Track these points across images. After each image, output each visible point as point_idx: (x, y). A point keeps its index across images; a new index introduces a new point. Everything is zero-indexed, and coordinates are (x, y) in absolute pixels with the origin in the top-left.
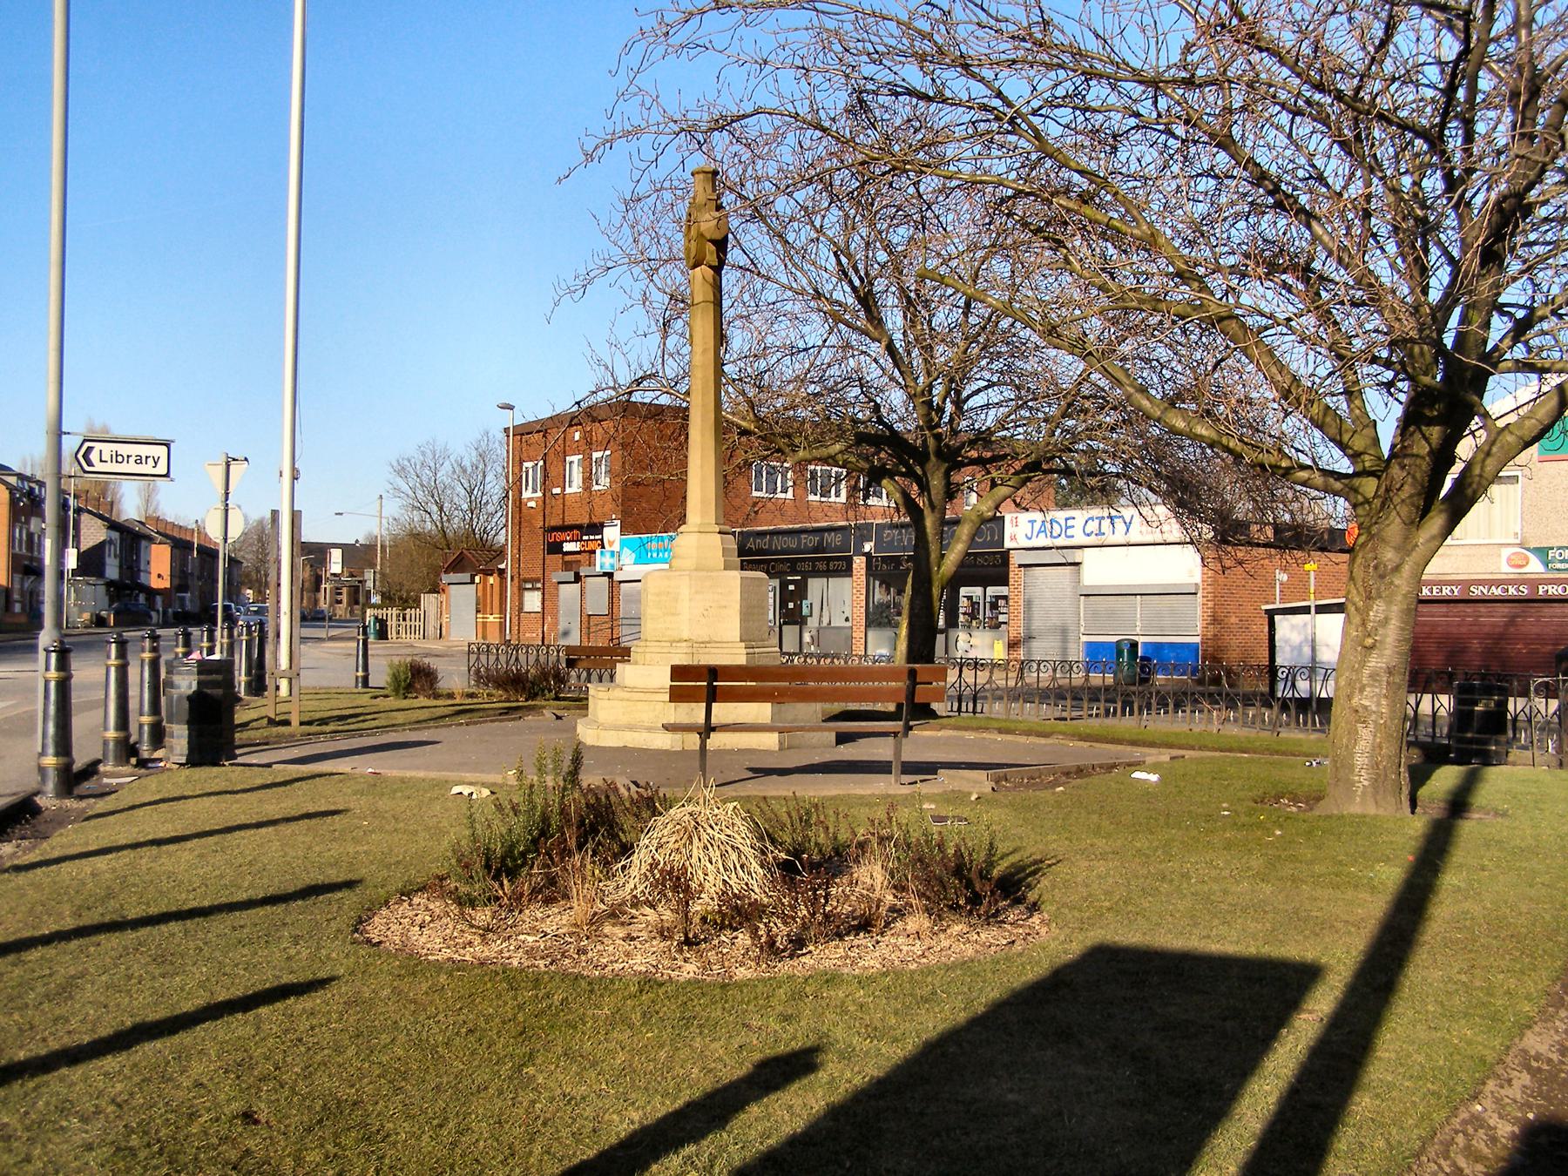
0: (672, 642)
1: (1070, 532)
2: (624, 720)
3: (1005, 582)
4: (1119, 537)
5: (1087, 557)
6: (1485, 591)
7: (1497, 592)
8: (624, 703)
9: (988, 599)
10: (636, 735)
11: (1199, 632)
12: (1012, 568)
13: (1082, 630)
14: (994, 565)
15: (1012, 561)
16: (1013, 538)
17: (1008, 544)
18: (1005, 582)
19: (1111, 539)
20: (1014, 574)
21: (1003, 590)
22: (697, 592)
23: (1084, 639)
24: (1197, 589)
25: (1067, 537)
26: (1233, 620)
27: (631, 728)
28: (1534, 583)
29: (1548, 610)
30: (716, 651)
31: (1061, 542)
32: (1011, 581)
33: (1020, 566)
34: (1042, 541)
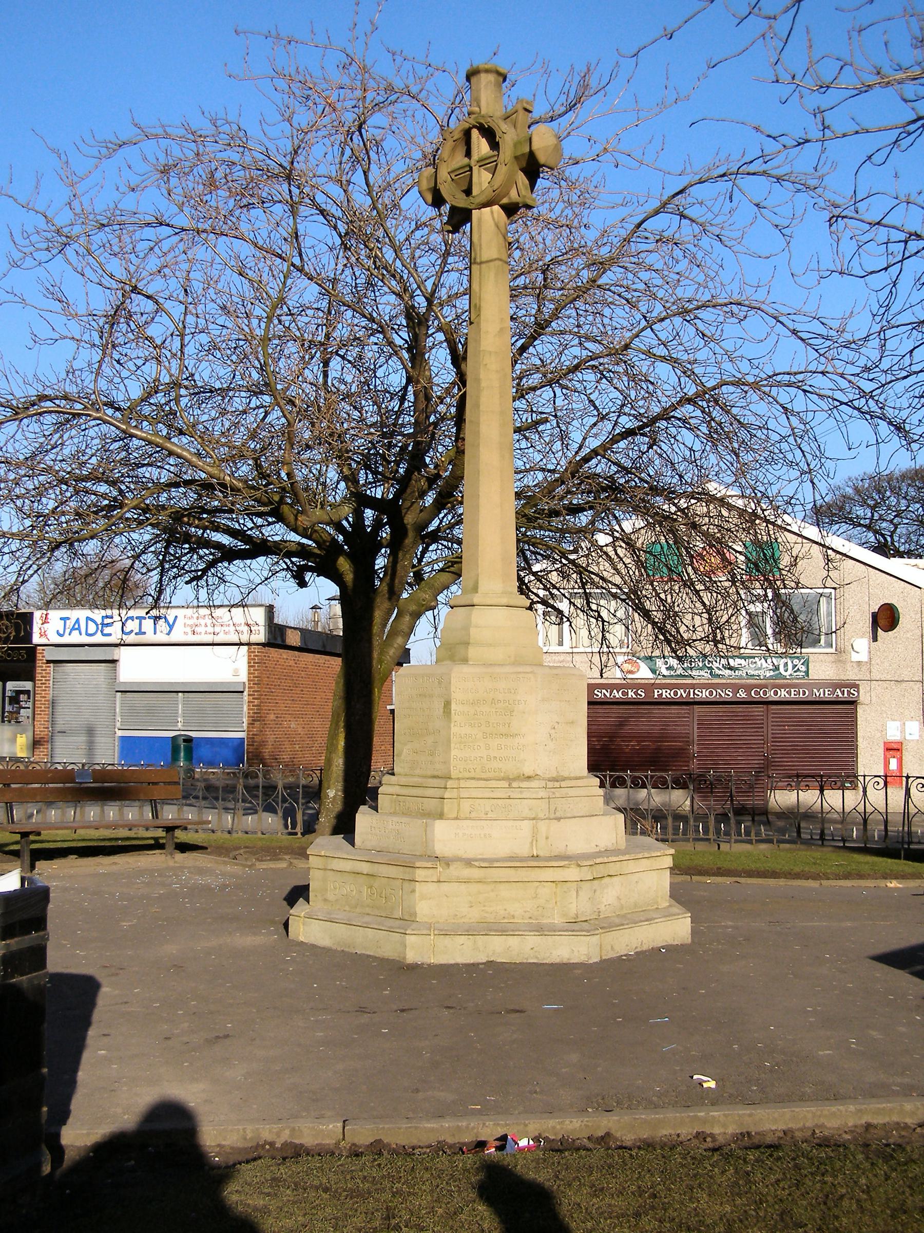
0: (510, 780)
1: (107, 630)
2: (474, 915)
3: (31, 677)
4: (161, 638)
5: (124, 654)
6: (608, 695)
7: (618, 695)
8: (474, 888)
9: (8, 694)
10: (513, 941)
11: (245, 728)
12: (39, 663)
13: (118, 725)
14: (19, 660)
15: (39, 656)
16: (43, 634)
17: (36, 639)
18: (31, 677)
19: (150, 637)
20: (41, 668)
21: (27, 685)
22: (543, 700)
23: (120, 733)
24: (244, 688)
25: (104, 635)
26: (272, 717)
27: (503, 929)
28: (649, 687)
29: (657, 711)
30: (572, 792)
31: (99, 639)
32: (38, 677)
33: (49, 662)
34: (75, 638)
